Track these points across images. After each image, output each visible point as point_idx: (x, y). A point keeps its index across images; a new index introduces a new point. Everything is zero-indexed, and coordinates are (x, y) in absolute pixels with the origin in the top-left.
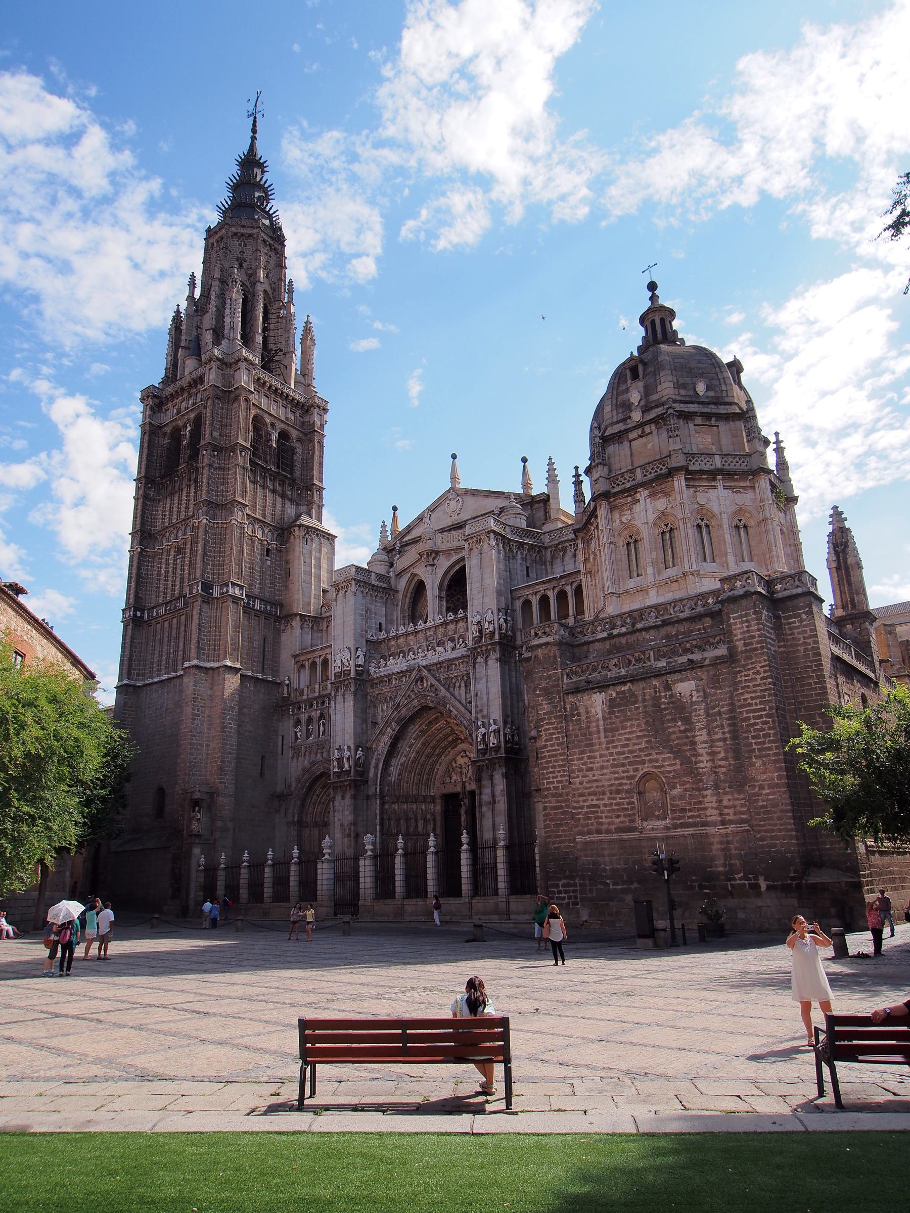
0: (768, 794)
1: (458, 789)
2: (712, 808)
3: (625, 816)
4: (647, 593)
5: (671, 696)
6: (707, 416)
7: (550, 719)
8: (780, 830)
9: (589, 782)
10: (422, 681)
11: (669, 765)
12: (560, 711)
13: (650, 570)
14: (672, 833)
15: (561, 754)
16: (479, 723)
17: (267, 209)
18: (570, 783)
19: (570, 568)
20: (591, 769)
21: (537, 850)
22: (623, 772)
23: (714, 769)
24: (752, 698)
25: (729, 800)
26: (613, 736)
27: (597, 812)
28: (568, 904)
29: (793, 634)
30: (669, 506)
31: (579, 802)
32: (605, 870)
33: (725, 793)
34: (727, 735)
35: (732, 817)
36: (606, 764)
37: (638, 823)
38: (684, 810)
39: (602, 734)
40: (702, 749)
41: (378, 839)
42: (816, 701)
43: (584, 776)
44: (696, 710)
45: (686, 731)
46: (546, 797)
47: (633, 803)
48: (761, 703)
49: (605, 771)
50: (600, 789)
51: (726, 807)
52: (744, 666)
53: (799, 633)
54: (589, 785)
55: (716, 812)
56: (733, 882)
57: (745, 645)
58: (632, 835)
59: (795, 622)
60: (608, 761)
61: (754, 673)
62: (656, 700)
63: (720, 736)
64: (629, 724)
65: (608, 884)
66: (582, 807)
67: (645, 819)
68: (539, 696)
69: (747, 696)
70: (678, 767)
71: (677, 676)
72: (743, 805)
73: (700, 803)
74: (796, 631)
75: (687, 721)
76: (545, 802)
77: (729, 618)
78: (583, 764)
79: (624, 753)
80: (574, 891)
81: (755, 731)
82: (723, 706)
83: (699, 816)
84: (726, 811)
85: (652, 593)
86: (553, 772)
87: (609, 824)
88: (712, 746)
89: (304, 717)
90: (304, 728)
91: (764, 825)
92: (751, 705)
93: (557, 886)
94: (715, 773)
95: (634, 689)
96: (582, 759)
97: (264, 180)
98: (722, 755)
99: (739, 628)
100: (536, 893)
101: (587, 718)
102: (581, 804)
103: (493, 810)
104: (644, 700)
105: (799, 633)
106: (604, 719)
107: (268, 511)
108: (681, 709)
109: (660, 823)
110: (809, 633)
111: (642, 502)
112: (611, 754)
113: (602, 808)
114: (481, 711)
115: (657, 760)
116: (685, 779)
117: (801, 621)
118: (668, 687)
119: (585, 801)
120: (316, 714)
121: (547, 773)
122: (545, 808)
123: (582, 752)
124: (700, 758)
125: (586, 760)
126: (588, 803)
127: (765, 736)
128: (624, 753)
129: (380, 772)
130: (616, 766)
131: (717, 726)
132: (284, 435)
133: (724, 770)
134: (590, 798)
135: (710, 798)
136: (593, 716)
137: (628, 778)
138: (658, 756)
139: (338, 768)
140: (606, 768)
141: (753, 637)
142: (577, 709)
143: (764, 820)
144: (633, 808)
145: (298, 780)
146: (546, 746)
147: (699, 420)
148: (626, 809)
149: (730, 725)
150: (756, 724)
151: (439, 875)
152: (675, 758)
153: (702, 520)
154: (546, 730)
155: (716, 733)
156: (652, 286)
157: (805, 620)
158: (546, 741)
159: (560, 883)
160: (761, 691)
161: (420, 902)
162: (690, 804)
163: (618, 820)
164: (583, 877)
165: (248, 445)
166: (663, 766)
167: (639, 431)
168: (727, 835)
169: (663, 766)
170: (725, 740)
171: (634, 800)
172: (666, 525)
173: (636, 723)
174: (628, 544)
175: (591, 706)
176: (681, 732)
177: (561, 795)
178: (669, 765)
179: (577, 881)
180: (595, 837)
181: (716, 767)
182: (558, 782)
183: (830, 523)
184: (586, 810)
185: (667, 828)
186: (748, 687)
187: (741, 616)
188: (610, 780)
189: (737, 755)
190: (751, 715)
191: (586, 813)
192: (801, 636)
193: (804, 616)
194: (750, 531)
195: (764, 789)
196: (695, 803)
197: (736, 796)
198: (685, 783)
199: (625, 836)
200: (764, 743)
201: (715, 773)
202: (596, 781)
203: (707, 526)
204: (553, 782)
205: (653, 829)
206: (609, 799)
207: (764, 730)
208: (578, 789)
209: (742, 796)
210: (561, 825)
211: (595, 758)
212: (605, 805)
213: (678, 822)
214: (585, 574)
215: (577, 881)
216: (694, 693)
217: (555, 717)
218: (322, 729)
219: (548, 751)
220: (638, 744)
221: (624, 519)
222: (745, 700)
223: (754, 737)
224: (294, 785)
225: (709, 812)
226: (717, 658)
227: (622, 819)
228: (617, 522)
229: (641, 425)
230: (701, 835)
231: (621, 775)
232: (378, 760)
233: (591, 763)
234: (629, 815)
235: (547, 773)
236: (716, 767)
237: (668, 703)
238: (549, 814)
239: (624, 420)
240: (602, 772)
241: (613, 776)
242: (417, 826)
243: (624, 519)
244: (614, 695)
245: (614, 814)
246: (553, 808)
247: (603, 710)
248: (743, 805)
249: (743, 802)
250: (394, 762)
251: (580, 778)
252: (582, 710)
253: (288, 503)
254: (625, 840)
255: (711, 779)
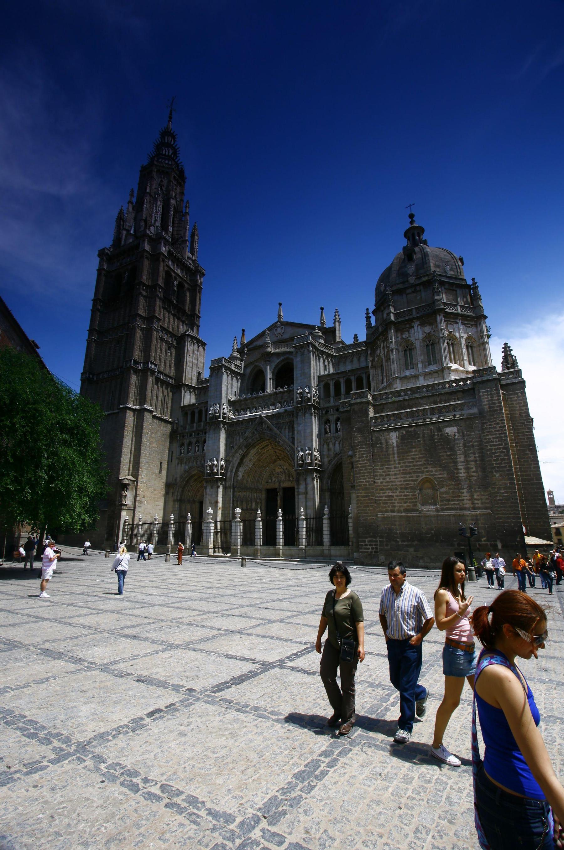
0: (503, 493)
1: (276, 486)
2: (467, 500)
3: (410, 502)
4: (418, 378)
5: (441, 435)
6: (451, 284)
7: (362, 445)
8: (510, 514)
9: (387, 482)
10: (262, 424)
11: (440, 474)
12: (369, 441)
13: (420, 366)
14: (441, 513)
15: (369, 466)
16: (299, 449)
17: (176, 160)
18: (374, 482)
19: (363, 364)
20: (389, 475)
21: (350, 521)
22: (410, 477)
23: (469, 477)
24: (493, 438)
25: (478, 495)
26: (403, 456)
27: (392, 500)
28: (371, 552)
29: (513, 404)
30: (432, 331)
31: (380, 493)
32: (396, 533)
33: (476, 492)
34: (477, 459)
35: (480, 505)
36: (398, 472)
37: (420, 507)
38: (449, 500)
39: (396, 456)
40: (461, 466)
41: (220, 512)
42: (527, 442)
43: (384, 479)
44: (457, 444)
45: (451, 455)
46: (359, 490)
47: (416, 495)
48: (499, 441)
49: (398, 476)
50: (394, 487)
51: (476, 499)
52: (489, 420)
53: (516, 404)
54: (386, 484)
55: (470, 502)
56: (480, 543)
57: (489, 407)
58: (414, 514)
59: (514, 397)
60: (400, 470)
61: (495, 424)
62: (432, 438)
63: (472, 458)
64: (414, 450)
65: (399, 542)
66: (382, 497)
67: (423, 505)
68: (355, 432)
69: (490, 437)
70: (445, 476)
71: (446, 424)
72: (487, 499)
73: (459, 496)
74: (515, 402)
75: (452, 449)
76: (358, 493)
77: (479, 392)
78: (383, 472)
79: (410, 466)
80: (375, 545)
81: (495, 456)
82: (475, 442)
83: (458, 504)
84: (476, 502)
85: (421, 378)
86: (364, 476)
87: (400, 506)
88: (467, 464)
89: (186, 442)
90: (186, 448)
91: (501, 511)
92: (493, 442)
93: (365, 541)
94: (469, 479)
95: (417, 430)
96: (383, 469)
97: (175, 144)
98: (474, 469)
99: (486, 398)
100: (349, 545)
101: (386, 446)
102: (382, 495)
103: (306, 498)
104: (424, 437)
105: (516, 404)
106: (397, 446)
107: (171, 325)
108: (448, 442)
109: (433, 507)
110: (523, 404)
111: (415, 328)
112: (402, 467)
113: (395, 498)
114: (300, 442)
115: (432, 471)
116: (450, 482)
117: (518, 397)
118: (439, 430)
119: (384, 493)
120: (194, 440)
121: (360, 477)
122: (358, 497)
123: (383, 465)
124: (460, 471)
125: (385, 470)
126: (385, 495)
127: (502, 460)
128: (410, 466)
129: (233, 474)
130: (405, 473)
131: (471, 453)
132: (181, 285)
133: (475, 478)
134: (387, 492)
135: (465, 494)
136: (391, 445)
137: (412, 481)
138: (432, 469)
139: (210, 470)
140: (399, 474)
141: (495, 403)
142: (380, 440)
143: (501, 507)
144: (415, 498)
145: (181, 477)
146: (359, 461)
147: (447, 286)
148: (411, 499)
149: (479, 453)
150: (497, 453)
151: (193, 534)
152: (443, 471)
153: (450, 340)
154: (359, 452)
155: (470, 457)
156: (411, 216)
157: (520, 396)
158: (359, 458)
159: (367, 540)
160: (500, 434)
161: (272, 548)
162: (452, 497)
163: (405, 505)
164: (381, 537)
165: (163, 285)
166: (436, 475)
167: (413, 289)
168: (476, 515)
169: (436, 475)
170: (476, 461)
171: (416, 493)
172: (430, 341)
173: (418, 449)
174: (405, 351)
175: (389, 439)
176: (447, 455)
177: (368, 489)
178: (440, 474)
179: (378, 539)
180: (390, 514)
181: (470, 476)
182: (367, 482)
183: (503, 352)
184: (384, 498)
185: (437, 510)
186: (491, 431)
187: (487, 391)
188: (401, 481)
189: (484, 470)
190: (493, 447)
191: (385, 500)
192: (518, 405)
193: (520, 395)
194: (475, 349)
195: (501, 490)
196: (455, 497)
197: (482, 493)
198: (450, 485)
199: (410, 514)
200: (501, 464)
201: (469, 479)
202: (392, 482)
203: (452, 344)
204: (363, 482)
205: (428, 511)
206: (400, 492)
207: (501, 456)
208: (379, 486)
209: (487, 493)
210: (368, 506)
211: (391, 468)
212: (397, 496)
213: (445, 507)
214: (371, 367)
215: (378, 539)
216: (456, 434)
217: (365, 445)
218: (197, 448)
219: (360, 464)
220: (419, 461)
221: (404, 337)
222: (490, 439)
223: (494, 460)
224: (178, 479)
225: (466, 502)
226: (471, 414)
227: (408, 504)
228: (400, 337)
229: (414, 286)
230: (460, 515)
231: (408, 479)
232: (233, 467)
233: (389, 471)
234: (413, 502)
235: (360, 477)
236: (470, 476)
237: (440, 439)
238: (361, 500)
239: (403, 283)
240: (396, 477)
241: (402, 479)
242: (251, 506)
243: (404, 337)
244: (404, 432)
245: (403, 501)
246: (363, 497)
247: (397, 441)
248: (487, 499)
249: (487, 497)
250: (241, 469)
251: (381, 480)
252: (383, 441)
253: (181, 323)
254: (410, 517)
255: (467, 483)
